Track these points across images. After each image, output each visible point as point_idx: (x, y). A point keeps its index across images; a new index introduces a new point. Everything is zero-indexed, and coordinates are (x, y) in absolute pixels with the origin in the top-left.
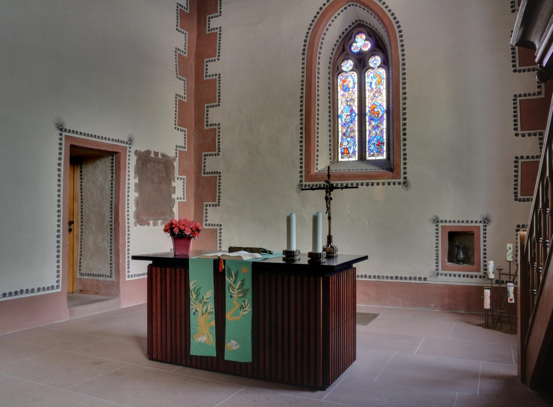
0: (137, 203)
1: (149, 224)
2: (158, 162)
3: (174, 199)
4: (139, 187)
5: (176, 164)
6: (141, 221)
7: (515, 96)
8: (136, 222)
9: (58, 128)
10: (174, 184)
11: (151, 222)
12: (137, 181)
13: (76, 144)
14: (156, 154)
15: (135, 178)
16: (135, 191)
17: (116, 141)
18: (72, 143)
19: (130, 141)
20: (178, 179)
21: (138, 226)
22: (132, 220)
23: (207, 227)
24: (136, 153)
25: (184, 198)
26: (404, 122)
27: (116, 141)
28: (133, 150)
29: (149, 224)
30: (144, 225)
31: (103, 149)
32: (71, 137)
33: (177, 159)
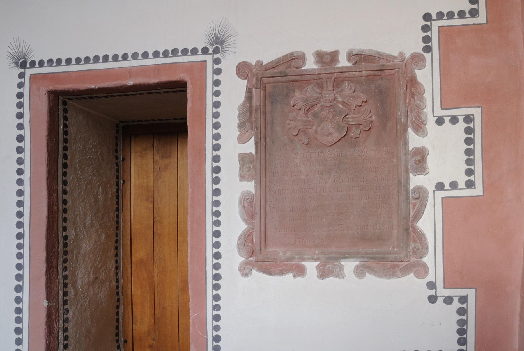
0: (249, 208)
1: (301, 271)
2: (338, 83)
3: (421, 194)
4: (259, 166)
5: (428, 77)
6: (261, 255)
7: (427, 17)
8: (246, 263)
9: (16, 63)
10: (414, 141)
11: (311, 266)
12: (250, 147)
13: (60, 87)
14: (327, 58)
15: (242, 140)
16: (242, 178)
17: (166, 54)
18: (51, 88)
19: (218, 44)
20: (440, 121)
21: (255, 273)
22: (232, 258)
23: (478, 178)
24: (243, 70)
25: (470, 184)
26: (216, 77)
27: (166, 54)
28: (229, 65)
29: (301, 271)
30: (282, 273)
31: (130, 83)
32: (44, 76)
33: (433, 59)
